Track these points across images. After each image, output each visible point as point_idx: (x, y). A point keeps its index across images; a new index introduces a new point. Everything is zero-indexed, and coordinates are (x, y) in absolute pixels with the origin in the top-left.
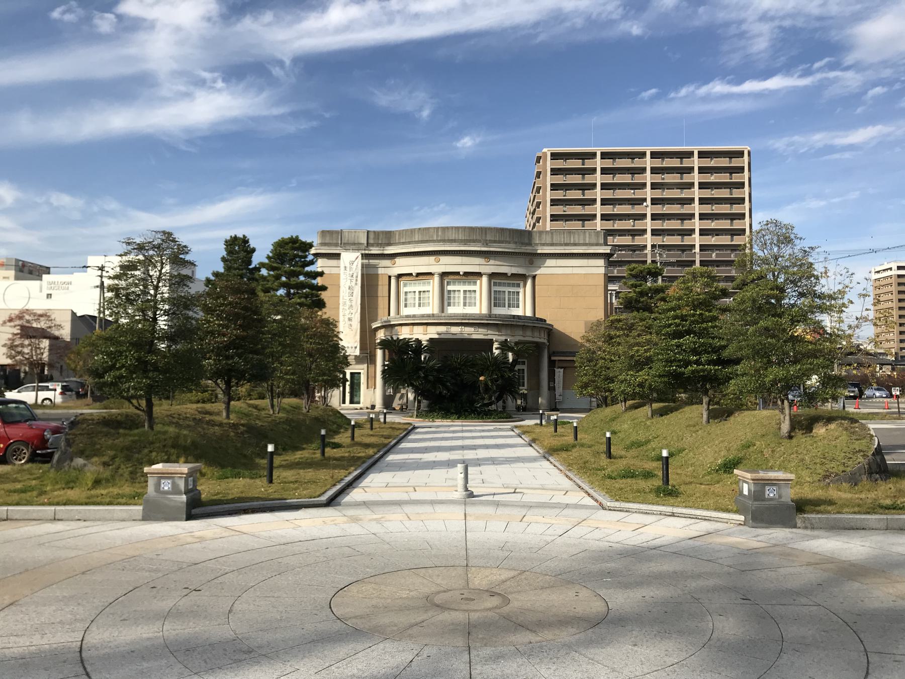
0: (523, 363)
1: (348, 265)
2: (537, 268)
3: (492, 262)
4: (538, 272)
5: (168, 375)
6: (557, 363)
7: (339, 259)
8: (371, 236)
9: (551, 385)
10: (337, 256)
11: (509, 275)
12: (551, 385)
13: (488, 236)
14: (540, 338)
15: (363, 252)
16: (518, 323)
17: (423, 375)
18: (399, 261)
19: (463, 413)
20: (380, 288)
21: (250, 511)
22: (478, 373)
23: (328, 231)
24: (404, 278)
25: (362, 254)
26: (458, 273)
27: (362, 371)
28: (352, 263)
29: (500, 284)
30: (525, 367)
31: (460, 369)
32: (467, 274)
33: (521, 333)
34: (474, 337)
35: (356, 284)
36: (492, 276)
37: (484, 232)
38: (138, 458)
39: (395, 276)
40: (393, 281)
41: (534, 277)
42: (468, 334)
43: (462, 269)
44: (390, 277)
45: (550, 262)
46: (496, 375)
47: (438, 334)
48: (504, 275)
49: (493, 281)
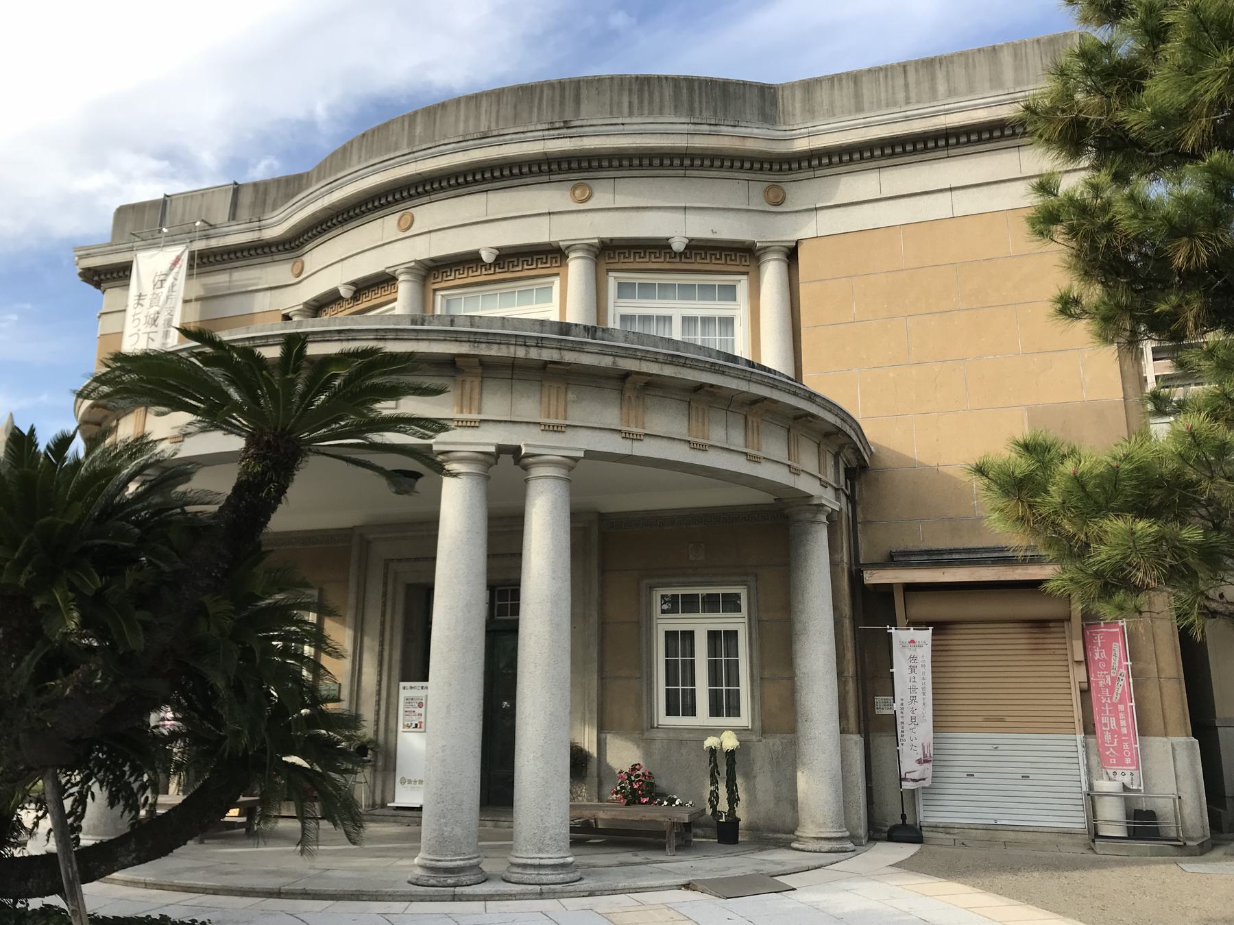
0: (731, 603)
1: (148, 289)
3: (602, 197)
4: (805, 229)
5: (299, 733)
11: (678, 245)
13: (583, 107)
15: (200, 245)
25: (192, 256)
29: (646, 290)
30: (737, 622)
32: (510, 257)
33: (611, 415)
37: (569, 93)
41: (791, 255)
43: (486, 241)
49: (612, 281)
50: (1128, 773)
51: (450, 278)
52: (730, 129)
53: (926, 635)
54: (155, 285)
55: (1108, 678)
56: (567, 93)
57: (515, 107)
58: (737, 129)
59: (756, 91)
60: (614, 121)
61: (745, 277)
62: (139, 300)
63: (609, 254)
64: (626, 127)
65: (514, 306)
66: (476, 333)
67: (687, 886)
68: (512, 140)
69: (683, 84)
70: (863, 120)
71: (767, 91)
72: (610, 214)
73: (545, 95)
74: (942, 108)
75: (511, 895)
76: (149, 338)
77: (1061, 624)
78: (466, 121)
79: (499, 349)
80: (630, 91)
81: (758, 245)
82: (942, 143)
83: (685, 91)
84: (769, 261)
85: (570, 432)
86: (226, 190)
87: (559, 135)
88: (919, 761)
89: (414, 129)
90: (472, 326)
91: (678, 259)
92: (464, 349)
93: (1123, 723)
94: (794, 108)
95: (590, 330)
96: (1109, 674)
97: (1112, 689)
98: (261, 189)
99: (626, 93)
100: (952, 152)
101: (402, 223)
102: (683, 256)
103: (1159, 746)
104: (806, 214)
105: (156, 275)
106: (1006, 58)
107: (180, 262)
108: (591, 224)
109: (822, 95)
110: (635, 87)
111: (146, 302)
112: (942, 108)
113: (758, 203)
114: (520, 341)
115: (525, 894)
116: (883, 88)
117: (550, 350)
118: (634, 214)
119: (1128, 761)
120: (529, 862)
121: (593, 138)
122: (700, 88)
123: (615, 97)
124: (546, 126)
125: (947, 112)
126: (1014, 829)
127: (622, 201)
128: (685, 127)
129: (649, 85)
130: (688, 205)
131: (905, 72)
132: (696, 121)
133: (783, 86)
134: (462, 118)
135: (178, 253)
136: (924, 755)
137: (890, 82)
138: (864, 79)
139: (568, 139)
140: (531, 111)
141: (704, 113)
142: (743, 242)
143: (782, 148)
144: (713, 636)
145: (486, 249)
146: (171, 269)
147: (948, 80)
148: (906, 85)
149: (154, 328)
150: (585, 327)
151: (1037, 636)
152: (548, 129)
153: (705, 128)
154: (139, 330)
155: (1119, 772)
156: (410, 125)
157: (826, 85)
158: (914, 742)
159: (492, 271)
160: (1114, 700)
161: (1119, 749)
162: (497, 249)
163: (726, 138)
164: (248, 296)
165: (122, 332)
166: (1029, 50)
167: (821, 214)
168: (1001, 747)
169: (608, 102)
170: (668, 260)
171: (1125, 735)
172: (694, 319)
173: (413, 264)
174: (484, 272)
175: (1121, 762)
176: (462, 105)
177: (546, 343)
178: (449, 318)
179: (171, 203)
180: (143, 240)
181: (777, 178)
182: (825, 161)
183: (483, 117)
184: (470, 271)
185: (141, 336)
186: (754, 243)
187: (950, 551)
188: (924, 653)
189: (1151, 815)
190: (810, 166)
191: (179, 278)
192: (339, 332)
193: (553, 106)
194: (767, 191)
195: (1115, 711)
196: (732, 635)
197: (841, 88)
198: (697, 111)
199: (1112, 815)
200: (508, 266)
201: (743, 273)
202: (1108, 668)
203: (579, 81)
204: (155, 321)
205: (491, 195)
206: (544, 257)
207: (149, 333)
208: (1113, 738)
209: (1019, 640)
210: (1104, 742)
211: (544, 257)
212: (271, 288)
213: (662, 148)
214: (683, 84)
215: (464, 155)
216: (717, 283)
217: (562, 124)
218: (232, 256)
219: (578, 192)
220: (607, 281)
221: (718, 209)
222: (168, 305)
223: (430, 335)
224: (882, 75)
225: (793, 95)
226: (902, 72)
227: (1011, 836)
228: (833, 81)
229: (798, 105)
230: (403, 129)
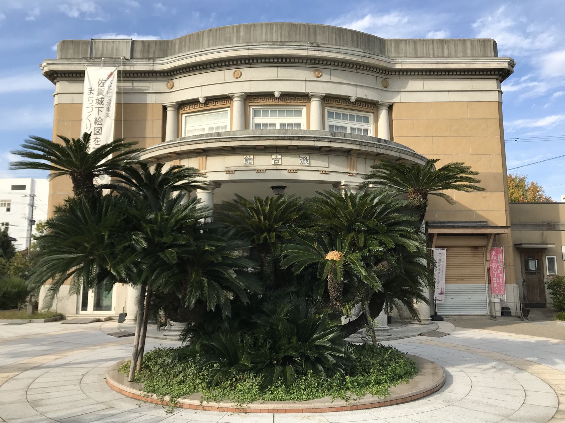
1: (95, 86)
2: (396, 94)
3: (326, 77)
4: (397, 99)
6: (435, 238)
7: (84, 83)
8: (138, 48)
10: (79, 76)
11: (353, 100)
13: (318, 37)
15: (121, 68)
17: (145, 244)
18: (181, 82)
19: (278, 369)
20: (149, 124)
22: (321, 243)
23: (72, 41)
24: (187, 109)
25: (119, 72)
26: (269, 95)
28: (102, 83)
29: (338, 116)
31: (269, 230)
32: (285, 96)
34: (303, 176)
35: (107, 115)
36: (327, 99)
37: (312, 30)
39: (173, 106)
40: (170, 114)
42: (290, 171)
43: (277, 88)
44: (165, 108)
45: (415, 84)
46: (381, 243)
47: (229, 172)
48: (344, 99)
50: (502, 295)
51: (257, 101)
52: (376, 56)
53: (444, 251)
54: (99, 85)
55: (496, 265)
56: (311, 30)
57: (289, 33)
58: (378, 57)
59: (378, 41)
60: (337, 47)
61: (372, 114)
62: (91, 91)
63: (326, 100)
64: (341, 50)
65: (285, 116)
66: (362, 142)
67: (420, 335)
68: (294, 48)
69: (355, 34)
70: (422, 61)
71: (382, 41)
72: (329, 84)
73: (302, 30)
74: (450, 61)
75: (380, 340)
76: (99, 110)
77: (482, 248)
78: (266, 34)
79: (368, 148)
80: (336, 33)
81: (380, 103)
82: (447, 73)
83: (355, 37)
84: (383, 109)
86: (127, 42)
87: (314, 49)
88: (440, 294)
89: (240, 33)
90: (351, 138)
92: (357, 147)
93: (501, 280)
94: (392, 50)
95: (386, 141)
96: (497, 264)
97: (498, 269)
98: (147, 44)
99: (334, 34)
100: (450, 77)
101: (236, 74)
102: (353, 104)
103: (509, 286)
104: (396, 93)
105: (100, 80)
106: (468, 44)
107: (113, 75)
108: (322, 87)
109: (402, 46)
110: (337, 32)
111: (95, 92)
112: (450, 61)
114: (375, 146)
115: (384, 339)
116: (425, 48)
117: (383, 150)
118: (338, 85)
119: (502, 292)
120: (380, 329)
121: (327, 52)
122: (360, 36)
123: (330, 36)
124: (310, 45)
125: (452, 63)
126: (468, 315)
127: (334, 79)
128: (361, 53)
129: (342, 32)
130: (358, 84)
131: (433, 43)
132: (365, 52)
133: (388, 40)
134: (264, 32)
135: (112, 71)
136: (442, 292)
137: (427, 46)
138: (418, 43)
139: (317, 52)
140: (296, 35)
141: (362, 47)
142: (374, 101)
143: (391, 66)
145: (278, 92)
146: (108, 78)
147: (448, 49)
148: (433, 49)
149: (101, 106)
150: (384, 140)
151: (474, 252)
152: (310, 46)
153: (368, 55)
154: (93, 106)
155: (499, 295)
156: (237, 31)
157: (404, 42)
158: (438, 287)
159: (277, 101)
160: (498, 273)
161: (499, 288)
162: (282, 92)
163: (374, 60)
164: (143, 94)
165: (82, 104)
166: (476, 43)
167: (402, 93)
168: (462, 289)
169: (327, 37)
170: (348, 105)
171: (501, 284)
172: (333, 126)
173: (243, 94)
174: (273, 101)
175: (499, 292)
176: (264, 27)
177: (382, 147)
178: (343, 134)
179: (95, 44)
180: (87, 61)
182: (405, 73)
183: (274, 34)
184: (267, 100)
185: (94, 108)
186: (378, 102)
187: (448, 222)
188: (444, 257)
189: (509, 309)
190: (399, 74)
191: (113, 83)
192: (314, 137)
193: (305, 35)
194: (383, 81)
195: (498, 276)
197: (409, 45)
198: (360, 46)
199: (498, 308)
200: (285, 100)
202: (497, 262)
203: (316, 26)
204: (102, 102)
205: (279, 69)
206: (300, 97)
207: (99, 108)
208: (497, 285)
209: (468, 253)
210: (494, 286)
211: (300, 97)
212: (156, 93)
213: (351, 60)
214: (355, 34)
215: (272, 51)
216: (362, 115)
217: (316, 45)
218: (135, 75)
219: (316, 73)
221: (367, 87)
222: (108, 95)
223: (336, 141)
224: (424, 42)
225: (391, 45)
226: (432, 43)
227: (466, 317)
228: (406, 42)
229: (393, 49)
230: (233, 32)
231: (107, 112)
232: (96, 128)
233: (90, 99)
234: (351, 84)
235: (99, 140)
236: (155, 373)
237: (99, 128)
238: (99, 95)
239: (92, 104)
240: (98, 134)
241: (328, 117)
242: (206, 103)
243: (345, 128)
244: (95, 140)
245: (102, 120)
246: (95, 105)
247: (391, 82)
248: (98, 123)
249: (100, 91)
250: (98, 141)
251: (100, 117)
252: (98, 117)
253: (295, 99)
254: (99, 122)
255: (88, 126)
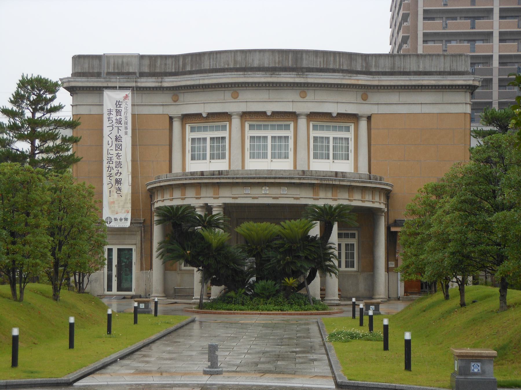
0: (353, 236)
1: (113, 108)
9: (390, 266)
11: (335, 115)
12: (390, 266)
14: (373, 202)
16: (342, 183)
21: (360, 73)
27: (133, 247)
30: (354, 241)
33: (346, 196)
38: (517, 279)
40: (177, 125)
44: (171, 119)
48: (327, 115)
54: (116, 106)
61: (353, 124)
64: (322, 76)
76: (118, 129)
85: (338, 200)
91: (333, 118)
92: (319, 182)
105: (117, 102)
113: (360, 100)
144: (347, 245)
149: (120, 125)
181: (366, 91)
196: (353, 245)
201: (353, 123)
204: (120, 122)
207: (118, 127)
220: (310, 125)
231: (125, 131)
232: (117, 145)
233: (110, 119)
234: (332, 102)
235: (120, 155)
236: (474, 209)
237: (119, 145)
238: (118, 116)
239: (112, 124)
240: (119, 149)
241: (313, 130)
242: (208, 117)
243: (328, 138)
244: (117, 155)
245: (121, 137)
246: (115, 125)
247: (370, 95)
248: (118, 140)
249: (117, 112)
250: (119, 157)
251: (120, 135)
252: (118, 135)
253: (284, 116)
254: (119, 139)
255: (110, 143)
